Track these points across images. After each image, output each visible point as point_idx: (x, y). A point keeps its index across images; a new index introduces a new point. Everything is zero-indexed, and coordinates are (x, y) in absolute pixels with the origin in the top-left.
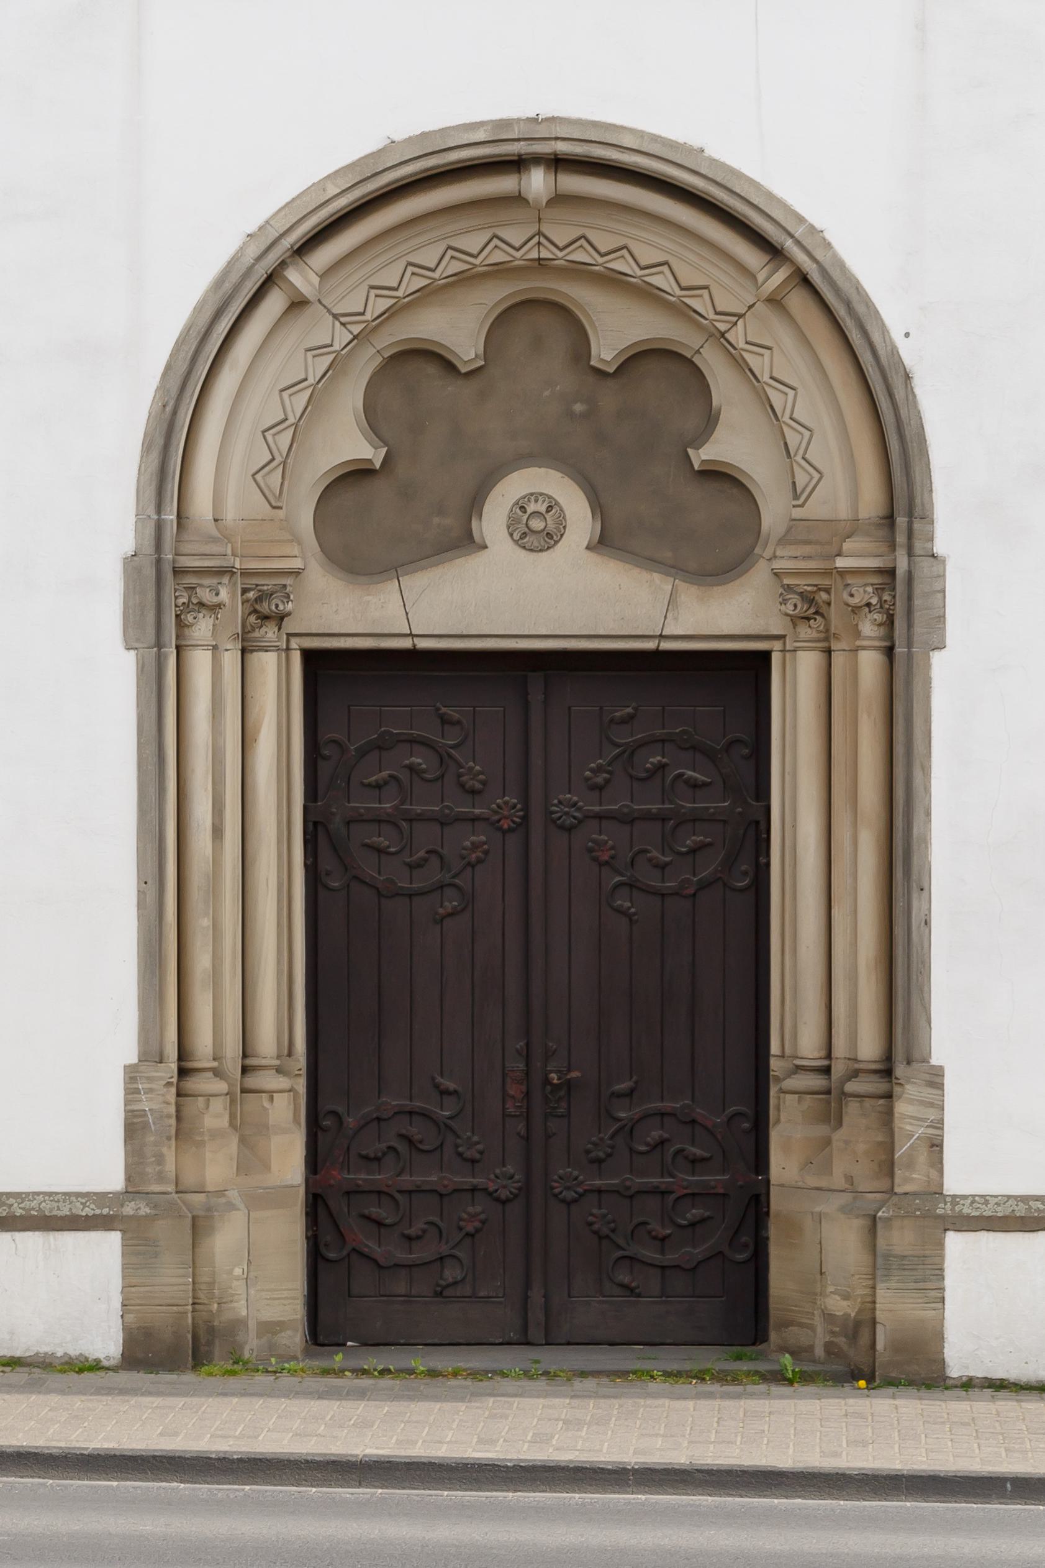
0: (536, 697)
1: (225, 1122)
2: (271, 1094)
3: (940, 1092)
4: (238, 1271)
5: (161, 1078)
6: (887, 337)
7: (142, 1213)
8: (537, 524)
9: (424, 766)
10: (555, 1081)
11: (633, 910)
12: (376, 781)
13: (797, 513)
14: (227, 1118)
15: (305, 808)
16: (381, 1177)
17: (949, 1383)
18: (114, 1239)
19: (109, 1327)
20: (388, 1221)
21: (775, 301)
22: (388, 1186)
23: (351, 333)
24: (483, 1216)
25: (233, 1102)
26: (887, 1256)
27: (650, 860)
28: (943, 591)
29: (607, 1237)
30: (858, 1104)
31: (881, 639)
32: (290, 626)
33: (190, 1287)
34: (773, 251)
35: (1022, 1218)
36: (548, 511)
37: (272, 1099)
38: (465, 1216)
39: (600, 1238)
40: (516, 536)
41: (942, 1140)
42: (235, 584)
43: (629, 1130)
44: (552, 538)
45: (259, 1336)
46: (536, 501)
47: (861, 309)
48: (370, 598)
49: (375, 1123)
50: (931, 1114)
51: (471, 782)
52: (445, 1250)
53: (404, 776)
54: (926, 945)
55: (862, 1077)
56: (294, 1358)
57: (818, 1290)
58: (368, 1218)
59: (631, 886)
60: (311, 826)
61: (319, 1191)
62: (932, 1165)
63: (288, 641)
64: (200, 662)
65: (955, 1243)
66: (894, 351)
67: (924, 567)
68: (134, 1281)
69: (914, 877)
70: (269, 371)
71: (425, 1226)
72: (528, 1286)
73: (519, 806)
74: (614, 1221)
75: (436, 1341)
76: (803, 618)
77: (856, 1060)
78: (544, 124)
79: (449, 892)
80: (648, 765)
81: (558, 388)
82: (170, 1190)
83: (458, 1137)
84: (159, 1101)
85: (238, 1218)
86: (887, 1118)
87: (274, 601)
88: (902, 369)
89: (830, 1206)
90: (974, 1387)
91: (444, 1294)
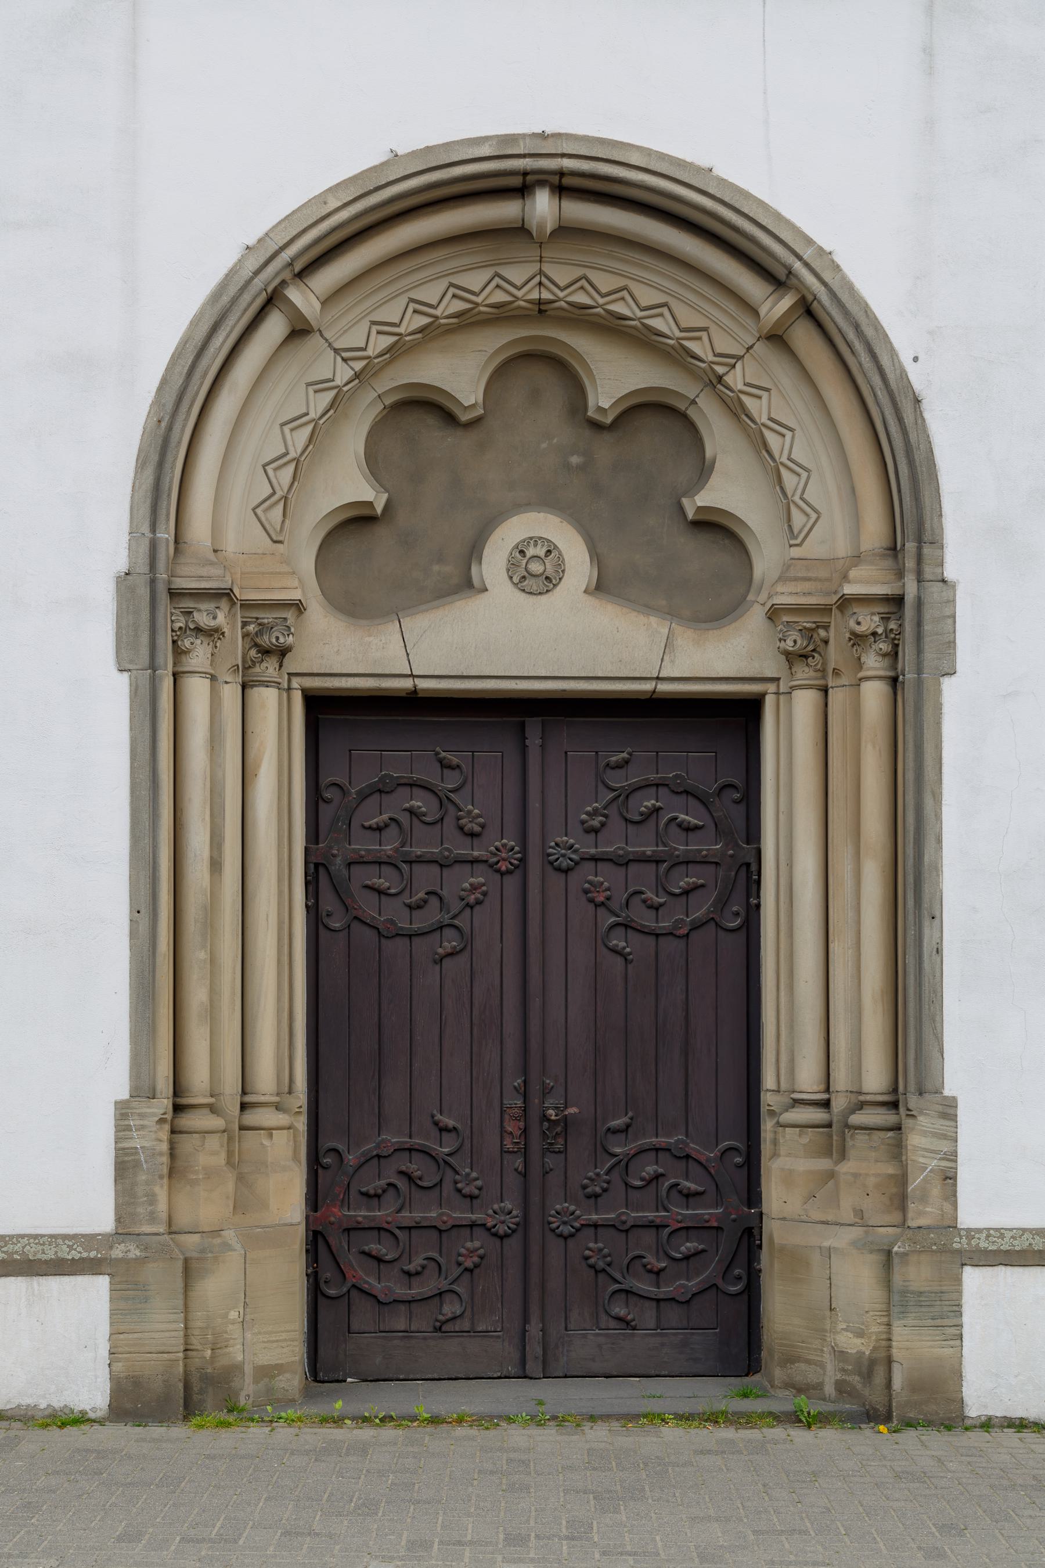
0: (534, 741)
1: (221, 1159)
2: (269, 1130)
3: (952, 1123)
4: (233, 1315)
5: (154, 1115)
6: (896, 361)
7: (131, 1255)
8: (536, 567)
9: (423, 809)
10: (553, 1118)
11: (628, 950)
12: (377, 823)
13: (795, 552)
14: (223, 1155)
15: (307, 850)
16: (382, 1213)
17: (968, 1422)
18: (102, 1283)
19: (96, 1377)
20: (388, 1258)
21: (777, 338)
22: (388, 1223)
23: (352, 369)
24: (481, 1252)
25: (230, 1139)
26: (904, 1293)
27: (644, 901)
28: (954, 617)
29: (604, 1270)
30: (867, 1137)
31: (885, 669)
32: (292, 664)
33: (182, 1333)
34: (777, 279)
35: (1040, 1251)
36: (546, 556)
37: (271, 1136)
38: (463, 1251)
39: (596, 1272)
40: (516, 579)
41: (956, 1173)
42: (234, 615)
43: (625, 1165)
44: (551, 581)
45: (256, 1381)
46: (536, 545)
47: (869, 332)
48: (371, 639)
49: (376, 1160)
50: (945, 1146)
51: (470, 825)
52: (444, 1285)
53: (404, 819)
54: (938, 974)
55: (868, 1110)
56: (291, 1402)
57: (828, 1327)
58: (368, 1255)
59: (626, 926)
60: (312, 866)
61: (320, 1228)
62: (946, 1199)
63: (289, 681)
64: (197, 689)
65: (972, 1278)
66: (903, 375)
67: (934, 591)
68: (122, 1328)
69: (925, 905)
70: (271, 407)
71: (425, 1262)
72: (526, 1319)
73: (517, 849)
74: (609, 1255)
75: (436, 1376)
76: (801, 656)
77: (860, 1093)
78: (550, 140)
79: (448, 933)
80: (643, 809)
81: (555, 441)
82: (162, 1230)
83: (457, 1173)
84: (151, 1139)
85: (234, 1258)
86: (898, 1151)
87: (276, 634)
88: (911, 392)
89: (841, 1239)
90: (993, 1426)
91: (443, 1329)
